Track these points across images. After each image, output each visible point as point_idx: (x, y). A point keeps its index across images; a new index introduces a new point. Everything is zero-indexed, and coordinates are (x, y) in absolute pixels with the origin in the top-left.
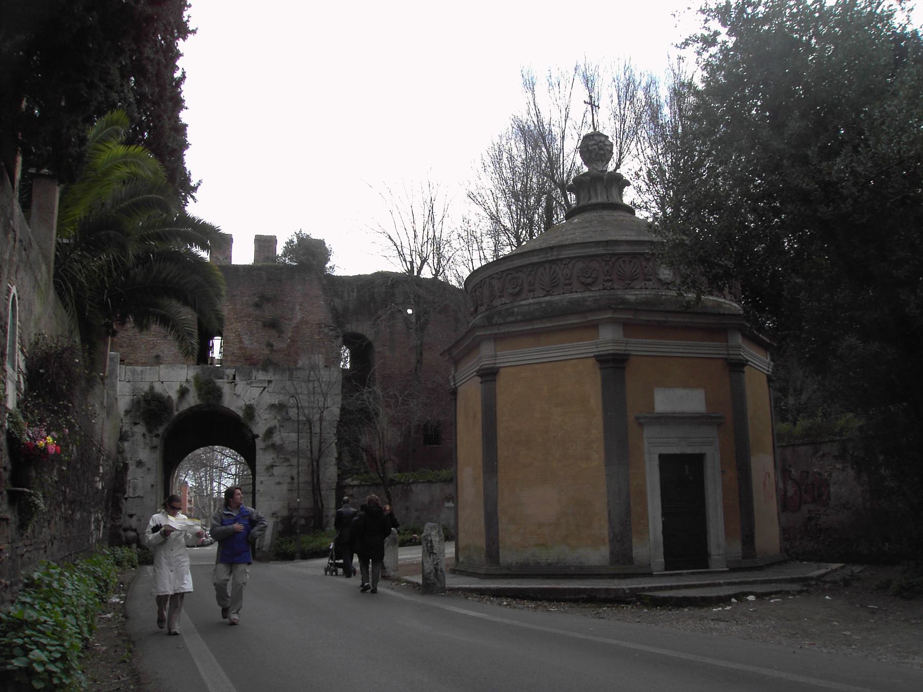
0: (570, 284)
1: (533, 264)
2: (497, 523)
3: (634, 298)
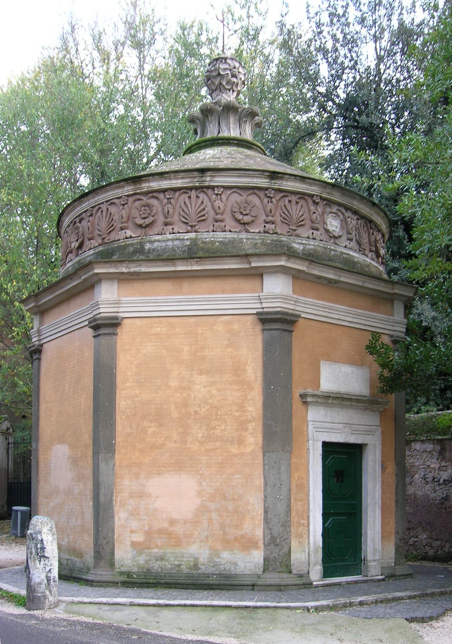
0: (222, 221)
1: (175, 190)
2: (113, 517)
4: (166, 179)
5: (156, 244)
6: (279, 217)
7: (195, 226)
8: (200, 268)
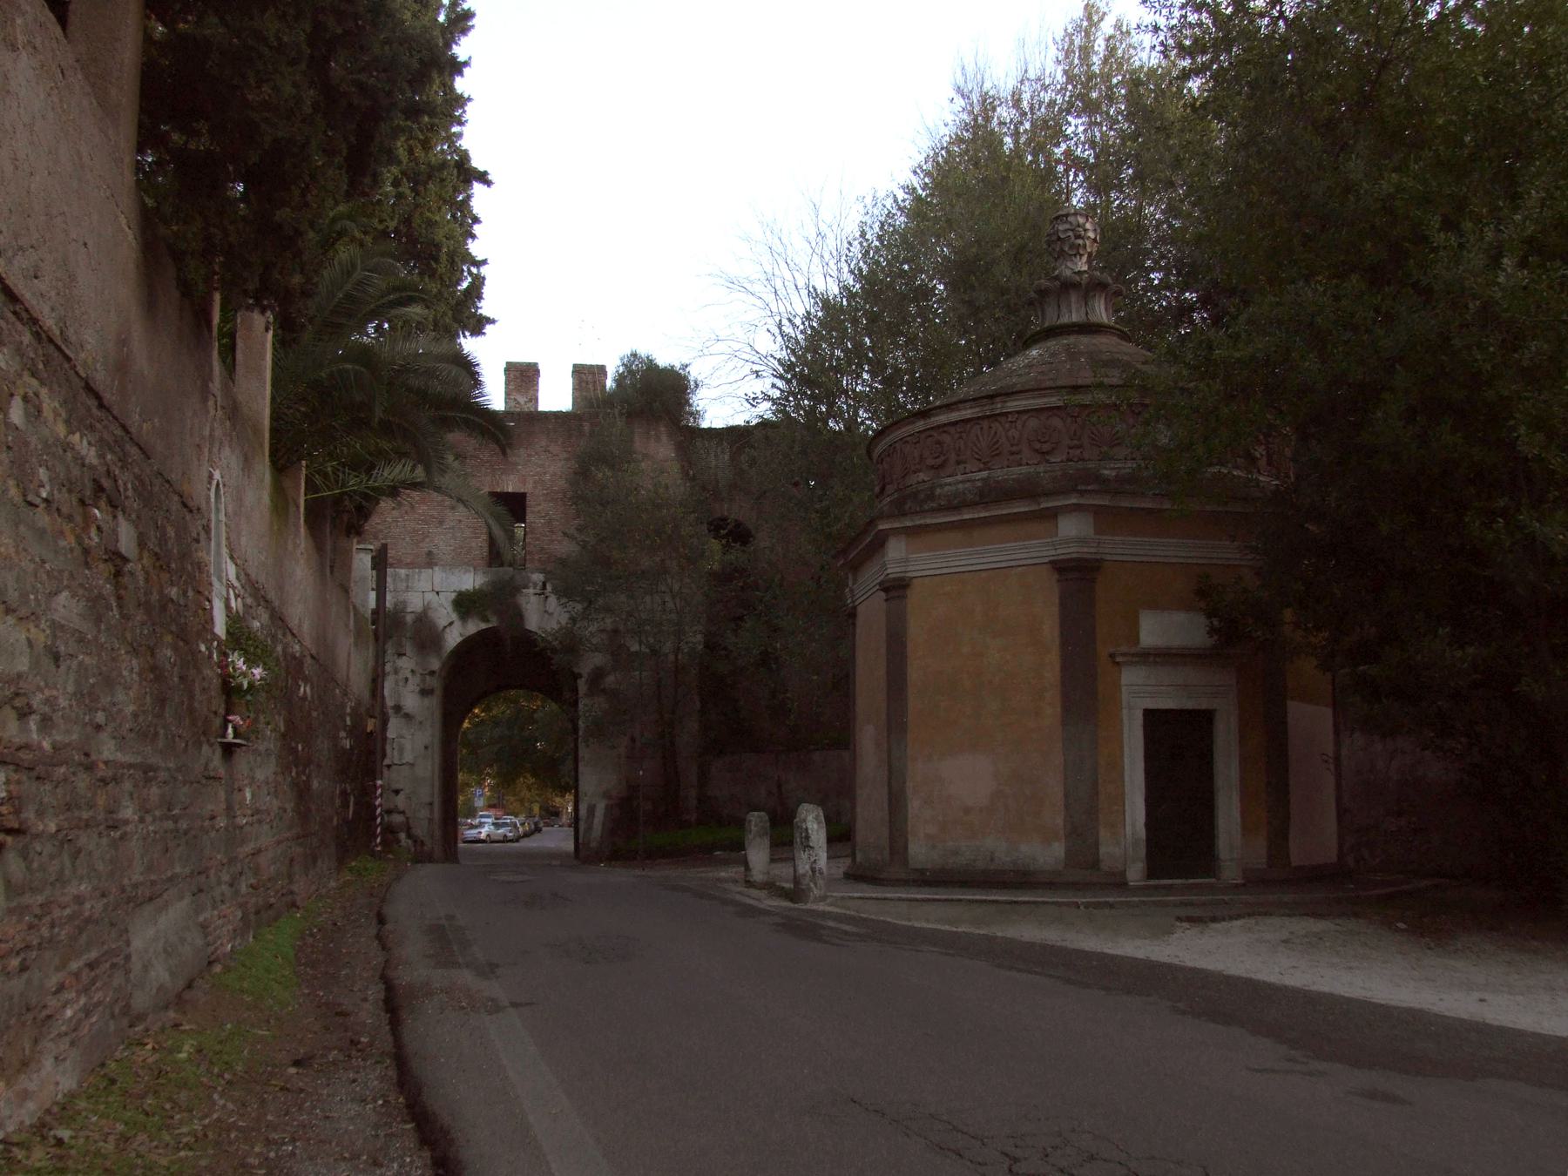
1: (968, 420)
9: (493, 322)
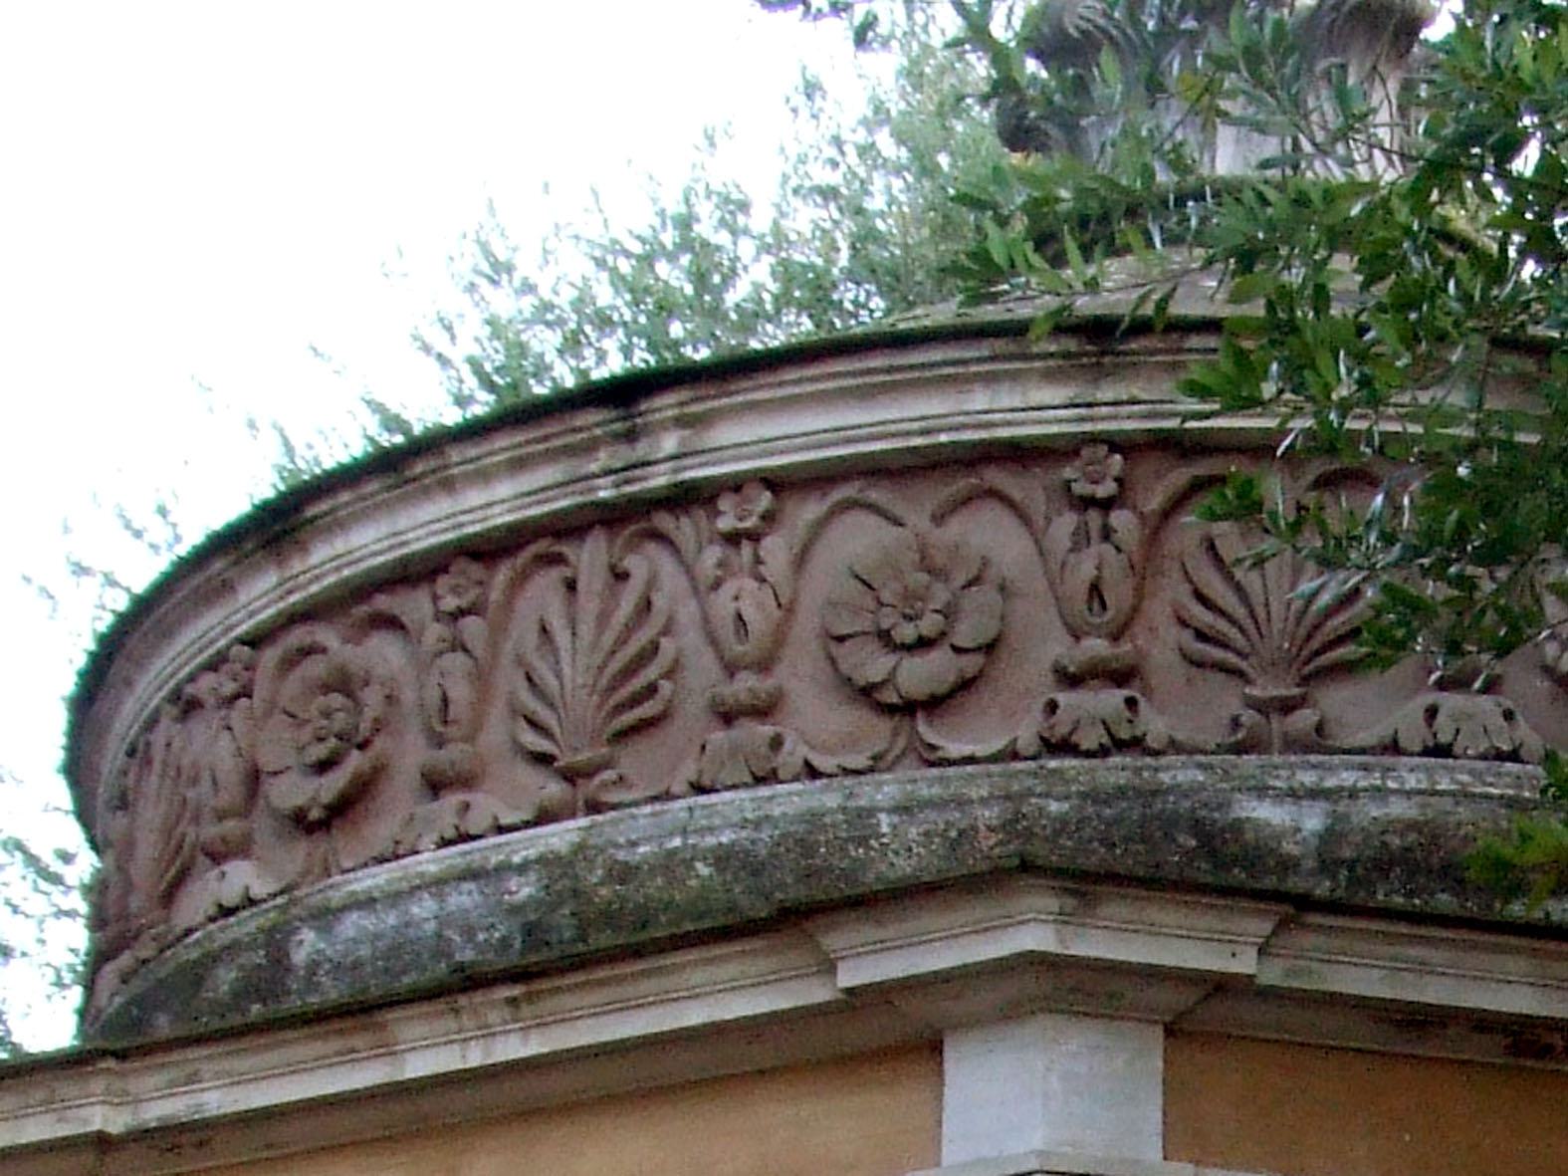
0: (763, 710)
1: (486, 550)
3: (1313, 820)
4: (426, 492)
5: (352, 925)
6: (1174, 635)
7: (588, 772)
8: (536, 1045)
9: (247, 888)
